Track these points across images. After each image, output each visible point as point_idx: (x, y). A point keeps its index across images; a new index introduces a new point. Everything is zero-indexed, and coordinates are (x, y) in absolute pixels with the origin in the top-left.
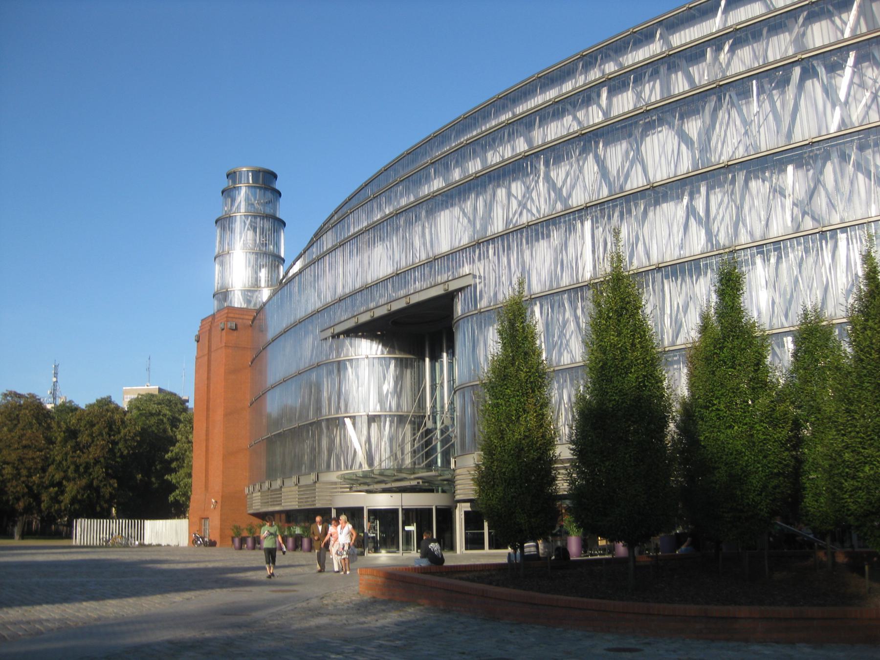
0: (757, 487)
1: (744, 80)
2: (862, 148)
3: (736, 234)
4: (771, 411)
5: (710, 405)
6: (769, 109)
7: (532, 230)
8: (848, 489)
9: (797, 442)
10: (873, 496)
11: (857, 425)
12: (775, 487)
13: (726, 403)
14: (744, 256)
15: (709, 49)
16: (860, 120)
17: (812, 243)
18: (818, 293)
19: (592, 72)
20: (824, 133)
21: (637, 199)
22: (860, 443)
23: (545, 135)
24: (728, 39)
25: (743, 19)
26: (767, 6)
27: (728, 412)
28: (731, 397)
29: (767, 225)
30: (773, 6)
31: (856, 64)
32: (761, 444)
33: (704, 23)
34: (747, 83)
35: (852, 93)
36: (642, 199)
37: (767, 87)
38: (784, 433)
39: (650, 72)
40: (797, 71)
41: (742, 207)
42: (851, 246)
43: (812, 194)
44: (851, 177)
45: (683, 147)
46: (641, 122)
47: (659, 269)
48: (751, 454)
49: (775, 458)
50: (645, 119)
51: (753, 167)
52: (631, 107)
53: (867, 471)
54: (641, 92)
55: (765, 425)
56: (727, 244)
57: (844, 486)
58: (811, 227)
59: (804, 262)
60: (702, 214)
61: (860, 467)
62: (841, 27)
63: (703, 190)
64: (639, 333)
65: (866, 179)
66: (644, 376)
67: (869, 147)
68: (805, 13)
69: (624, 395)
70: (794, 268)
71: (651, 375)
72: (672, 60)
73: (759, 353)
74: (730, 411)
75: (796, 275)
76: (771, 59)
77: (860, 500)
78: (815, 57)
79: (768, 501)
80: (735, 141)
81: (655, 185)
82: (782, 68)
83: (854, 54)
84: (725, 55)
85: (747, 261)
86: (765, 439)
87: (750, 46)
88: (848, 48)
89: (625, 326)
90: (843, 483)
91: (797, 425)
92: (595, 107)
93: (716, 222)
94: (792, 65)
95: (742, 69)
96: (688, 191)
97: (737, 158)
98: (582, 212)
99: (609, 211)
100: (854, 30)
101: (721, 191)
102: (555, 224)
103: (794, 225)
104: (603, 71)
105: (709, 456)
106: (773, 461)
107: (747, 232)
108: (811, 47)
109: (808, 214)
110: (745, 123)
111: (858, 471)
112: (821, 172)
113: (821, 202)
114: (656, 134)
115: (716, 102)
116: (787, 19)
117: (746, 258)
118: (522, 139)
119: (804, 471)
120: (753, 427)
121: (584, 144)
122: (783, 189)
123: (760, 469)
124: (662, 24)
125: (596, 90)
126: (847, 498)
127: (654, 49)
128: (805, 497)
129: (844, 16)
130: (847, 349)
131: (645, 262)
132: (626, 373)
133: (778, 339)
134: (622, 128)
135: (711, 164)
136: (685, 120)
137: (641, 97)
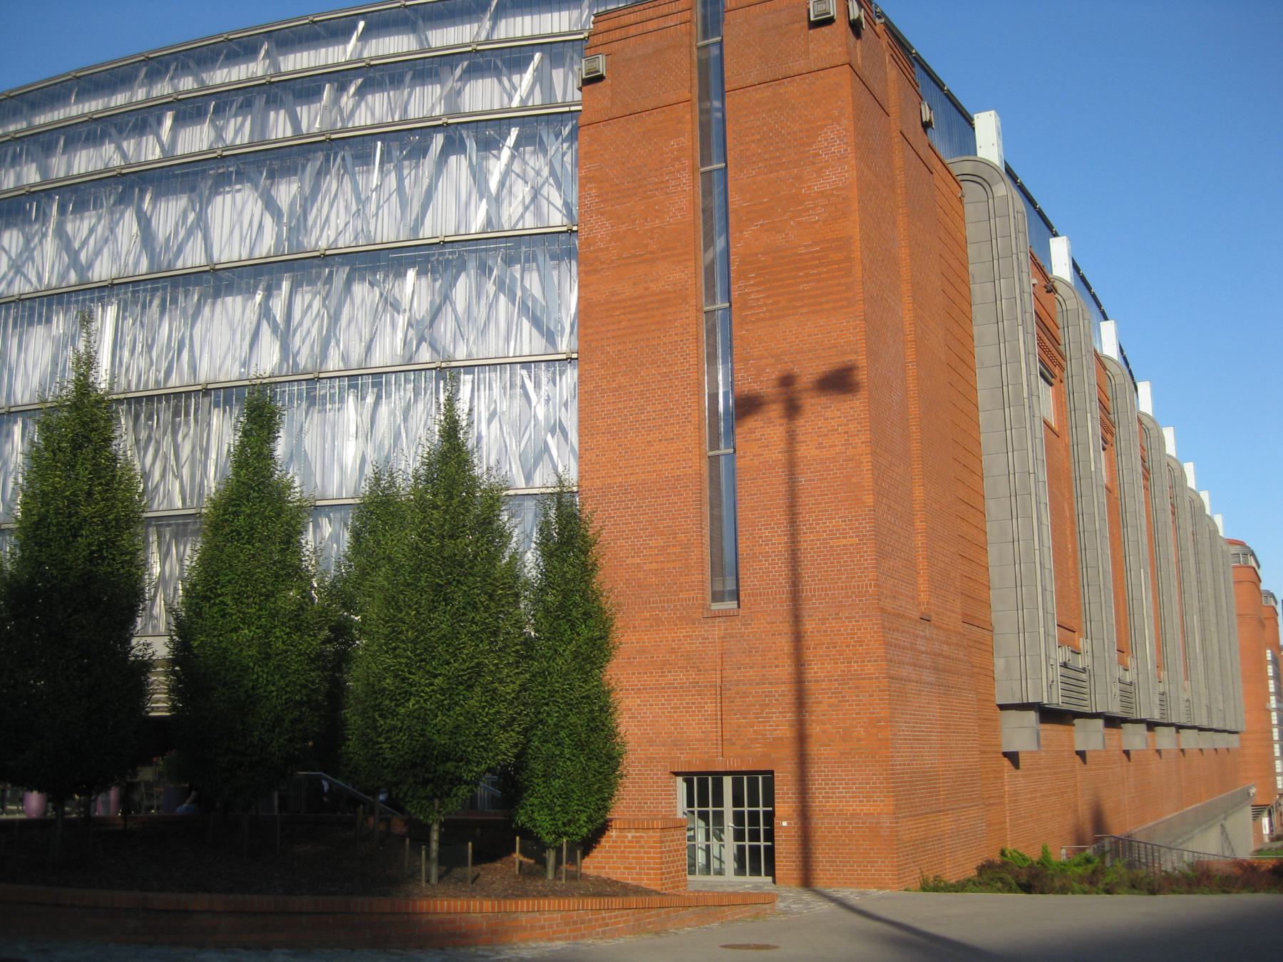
0: (267, 720)
1: (366, 138)
2: (509, 261)
6: (394, 185)
7: (24, 306)
10: (417, 741)
12: (294, 722)
14: (330, 387)
15: (327, 86)
16: (513, 222)
20: (462, 232)
22: (407, 665)
23: (70, 166)
26: (421, 43)
30: (428, 44)
36: (196, 285)
37: (396, 153)
39: (240, 102)
40: (438, 140)
43: (435, 313)
46: (211, 172)
47: (206, 392)
48: (262, 671)
50: (219, 168)
56: (309, 368)
63: (285, 286)
68: (466, 63)
69: (67, 569)
71: (113, 542)
77: (400, 746)
78: (466, 125)
81: (218, 267)
83: (517, 132)
85: (332, 396)
87: (386, 94)
90: (378, 721)
98: (107, 290)
102: (60, 303)
105: (203, 671)
106: (295, 682)
110: (362, 202)
111: (399, 705)
112: (452, 285)
113: (446, 327)
117: (332, 391)
118: (34, 166)
123: (274, 694)
126: (382, 743)
127: (256, 69)
128: (348, 740)
129: (516, 78)
132: (75, 536)
134: (183, 175)
135: (302, 250)
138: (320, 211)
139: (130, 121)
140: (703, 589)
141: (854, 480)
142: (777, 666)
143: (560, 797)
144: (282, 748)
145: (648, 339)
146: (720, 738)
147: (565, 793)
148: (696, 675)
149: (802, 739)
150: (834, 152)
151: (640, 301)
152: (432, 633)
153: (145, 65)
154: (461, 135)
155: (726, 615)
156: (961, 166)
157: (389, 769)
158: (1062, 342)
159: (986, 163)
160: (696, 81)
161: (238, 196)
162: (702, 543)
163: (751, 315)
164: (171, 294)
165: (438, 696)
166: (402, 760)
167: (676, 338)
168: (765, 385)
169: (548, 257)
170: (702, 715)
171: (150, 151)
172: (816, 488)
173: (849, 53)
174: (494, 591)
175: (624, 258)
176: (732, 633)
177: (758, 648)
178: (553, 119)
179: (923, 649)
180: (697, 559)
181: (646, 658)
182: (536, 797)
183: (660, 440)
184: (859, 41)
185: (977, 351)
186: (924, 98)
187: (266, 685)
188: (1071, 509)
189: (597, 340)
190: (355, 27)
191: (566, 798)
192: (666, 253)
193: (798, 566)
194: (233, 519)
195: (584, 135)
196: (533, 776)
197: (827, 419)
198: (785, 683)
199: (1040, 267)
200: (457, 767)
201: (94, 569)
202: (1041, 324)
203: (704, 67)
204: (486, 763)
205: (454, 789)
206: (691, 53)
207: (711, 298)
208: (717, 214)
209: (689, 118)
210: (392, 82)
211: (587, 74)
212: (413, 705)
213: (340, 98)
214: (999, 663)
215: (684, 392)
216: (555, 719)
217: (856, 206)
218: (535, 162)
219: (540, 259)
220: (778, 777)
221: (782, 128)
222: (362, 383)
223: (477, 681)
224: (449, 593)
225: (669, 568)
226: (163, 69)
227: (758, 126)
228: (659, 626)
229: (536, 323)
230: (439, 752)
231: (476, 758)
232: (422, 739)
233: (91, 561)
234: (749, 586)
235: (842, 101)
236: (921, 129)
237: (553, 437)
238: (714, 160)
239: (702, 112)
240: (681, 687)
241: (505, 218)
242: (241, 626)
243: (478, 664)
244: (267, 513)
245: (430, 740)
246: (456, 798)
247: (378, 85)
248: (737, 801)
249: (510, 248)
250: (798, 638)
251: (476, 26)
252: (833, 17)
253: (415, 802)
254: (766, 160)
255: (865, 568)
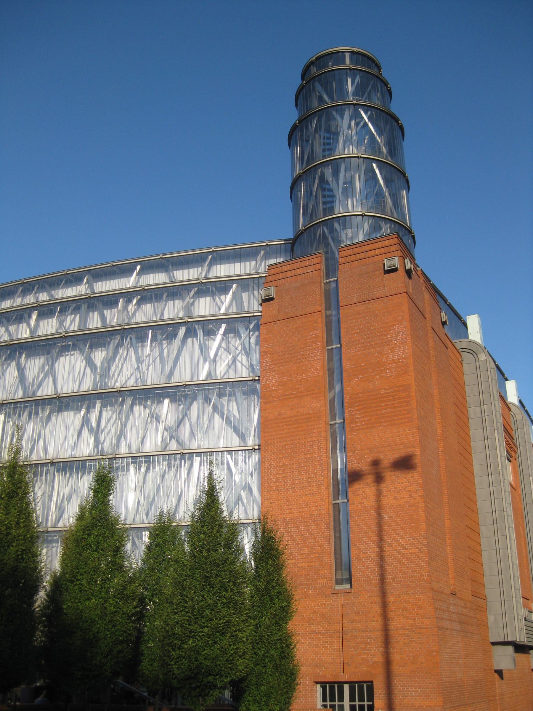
1: (144, 328)
2: (220, 396)
3: (118, 445)
4: (123, 589)
5: (75, 580)
8: (174, 657)
9: (141, 616)
10: (193, 664)
11: (187, 606)
12: (119, 652)
13: (87, 580)
14: (121, 463)
17: (174, 461)
18: (173, 500)
19: (28, 297)
21: (45, 404)
22: (188, 620)
24: (137, 295)
25: (151, 283)
26: (170, 278)
27: (88, 586)
28: (91, 575)
29: (142, 442)
31: (224, 334)
32: (112, 615)
33: (122, 279)
34: (145, 331)
35: (219, 354)
36: (48, 405)
37: (159, 337)
38: (131, 607)
39: (73, 307)
40: (183, 330)
41: (126, 425)
42: (202, 467)
43: (179, 423)
44: (210, 416)
45: (88, 370)
46: (59, 344)
47: (53, 463)
48: (102, 623)
49: (122, 627)
50: (63, 342)
51: (139, 396)
52: (54, 331)
53: (191, 644)
54: (63, 321)
55: (117, 600)
57: (171, 654)
58: (175, 448)
59: (166, 475)
60: (94, 424)
61: (185, 640)
62: (219, 304)
63: (98, 406)
64: (25, 514)
65: (220, 419)
66: (23, 550)
67: (225, 395)
68: (196, 289)
69: (4, 564)
70: (158, 478)
71: (29, 550)
72: (92, 302)
73: (119, 542)
74: (90, 586)
75: (159, 484)
76: (166, 317)
77: (182, 667)
78: (198, 322)
79: (112, 663)
80: (129, 373)
81: (61, 396)
82: (172, 325)
83: (225, 326)
84: (132, 307)
85: (123, 467)
86: (115, 612)
87: (153, 304)
88: (222, 321)
89: (13, 507)
90: (171, 652)
91: (142, 601)
92: (25, 325)
93: (103, 434)
94: (180, 324)
95: (144, 320)
96: (86, 405)
97: (128, 386)
99: (20, 410)
100: (227, 309)
101: (111, 410)
103: (163, 445)
104: (37, 298)
105: (69, 622)
106: (120, 629)
107: (126, 444)
108: (196, 314)
109: (174, 438)
110: (139, 361)
111: (184, 643)
112: (189, 408)
113: (185, 430)
114: (69, 356)
115: (119, 340)
116: (182, 290)
117: (123, 465)
119: (144, 640)
120: (107, 601)
121: (10, 353)
122: (159, 416)
123: (109, 636)
124: (90, 272)
125: (29, 311)
126: (173, 665)
128: (142, 662)
129: (223, 297)
130: (187, 548)
131: (42, 456)
132: (9, 546)
133: (138, 532)
136: (94, 350)
137: (63, 325)
138: (117, 367)
139: (13, 316)
140: (331, 578)
141: (415, 517)
142: (373, 621)
143: (265, 696)
144: (112, 667)
145: (299, 439)
146: (342, 662)
147: (268, 694)
148: (328, 626)
149: (388, 663)
150: (400, 339)
151: (295, 418)
152: (202, 603)
153: (22, 286)
154: (195, 328)
155: (346, 593)
156: (460, 344)
157: (176, 680)
158: (515, 438)
159: (474, 342)
160: (323, 301)
161: (72, 357)
162: (330, 552)
163: (356, 426)
164: (34, 409)
165: (206, 638)
166: (184, 675)
167: (314, 439)
168: (363, 466)
169: (241, 394)
170: (332, 649)
171: (24, 332)
172: (393, 521)
173: (406, 287)
174: (235, 580)
175: (286, 395)
176: (348, 602)
177: (363, 611)
178: (245, 320)
179: (453, 611)
180: (328, 560)
181: (300, 616)
182: (251, 696)
183: (306, 495)
184: (410, 280)
185: (472, 444)
186: (442, 309)
187: (104, 631)
188: (524, 530)
189: (271, 440)
190: (135, 268)
191: (268, 697)
192: (309, 393)
193: (385, 565)
194: (88, 538)
195: (263, 329)
196: (250, 684)
197: (399, 483)
198: (378, 630)
199: (503, 398)
200: (214, 679)
201: (19, 564)
202: (505, 430)
203: (327, 294)
204: (231, 677)
205: (211, 692)
206: (321, 287)
207: (333, 418)
208: (336, 372)
209: (320, 321)
210: (156, 298)
211: (265, 297)
212: (192, 643)
213: (128, 306)
214: (491, 619)
215: (319, 468)
216: (263, 652)
217: (412, 368)
218: (236, 343)
219: (238, 394)
220: (376, 684)
221: (371, 326)
222: (139, 461)
223: (226, 630)
224: (212, 581)
225: (312, 566)
226: (31, 289)
227: (358, 325)
228: (307, 598)
229: (236, 430)
230: (205, 671)
231: (225, 674)
232: (196, 663)
233: (17, 560)
234: (357, 576)
235: (403, 312)
236: (441, 325)
237: (244, 492)
238: (334, 342)
239: (327, 316)
240: (320, 633)
241: (218, 373)
242: (91, 597)
243: (227, 621)
244: (106, 535)
245: (201, 663)
246: (212, 697)
247: (149, 299)
248: (352, 699)
249: (221, 388)
250: (384, 605)
251: (200, 269)
252: (397, 268)
253: (189, 699)
254: (363, 343)
255: (422, 566)
